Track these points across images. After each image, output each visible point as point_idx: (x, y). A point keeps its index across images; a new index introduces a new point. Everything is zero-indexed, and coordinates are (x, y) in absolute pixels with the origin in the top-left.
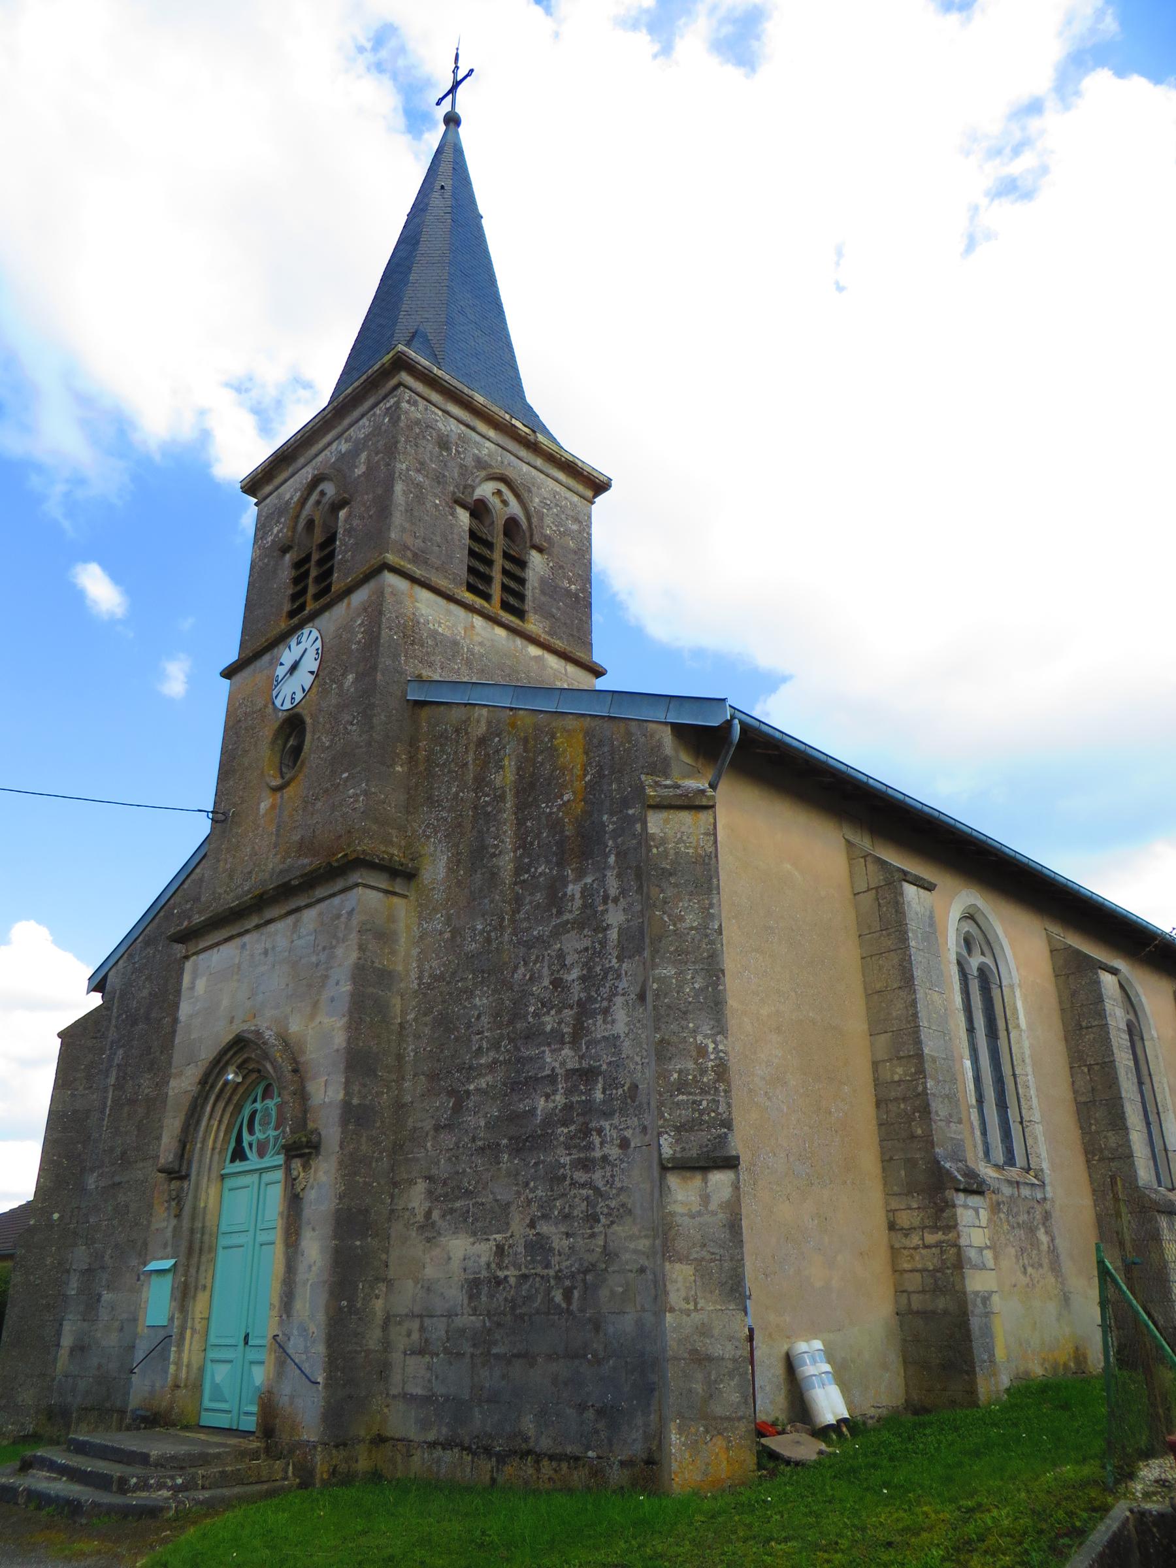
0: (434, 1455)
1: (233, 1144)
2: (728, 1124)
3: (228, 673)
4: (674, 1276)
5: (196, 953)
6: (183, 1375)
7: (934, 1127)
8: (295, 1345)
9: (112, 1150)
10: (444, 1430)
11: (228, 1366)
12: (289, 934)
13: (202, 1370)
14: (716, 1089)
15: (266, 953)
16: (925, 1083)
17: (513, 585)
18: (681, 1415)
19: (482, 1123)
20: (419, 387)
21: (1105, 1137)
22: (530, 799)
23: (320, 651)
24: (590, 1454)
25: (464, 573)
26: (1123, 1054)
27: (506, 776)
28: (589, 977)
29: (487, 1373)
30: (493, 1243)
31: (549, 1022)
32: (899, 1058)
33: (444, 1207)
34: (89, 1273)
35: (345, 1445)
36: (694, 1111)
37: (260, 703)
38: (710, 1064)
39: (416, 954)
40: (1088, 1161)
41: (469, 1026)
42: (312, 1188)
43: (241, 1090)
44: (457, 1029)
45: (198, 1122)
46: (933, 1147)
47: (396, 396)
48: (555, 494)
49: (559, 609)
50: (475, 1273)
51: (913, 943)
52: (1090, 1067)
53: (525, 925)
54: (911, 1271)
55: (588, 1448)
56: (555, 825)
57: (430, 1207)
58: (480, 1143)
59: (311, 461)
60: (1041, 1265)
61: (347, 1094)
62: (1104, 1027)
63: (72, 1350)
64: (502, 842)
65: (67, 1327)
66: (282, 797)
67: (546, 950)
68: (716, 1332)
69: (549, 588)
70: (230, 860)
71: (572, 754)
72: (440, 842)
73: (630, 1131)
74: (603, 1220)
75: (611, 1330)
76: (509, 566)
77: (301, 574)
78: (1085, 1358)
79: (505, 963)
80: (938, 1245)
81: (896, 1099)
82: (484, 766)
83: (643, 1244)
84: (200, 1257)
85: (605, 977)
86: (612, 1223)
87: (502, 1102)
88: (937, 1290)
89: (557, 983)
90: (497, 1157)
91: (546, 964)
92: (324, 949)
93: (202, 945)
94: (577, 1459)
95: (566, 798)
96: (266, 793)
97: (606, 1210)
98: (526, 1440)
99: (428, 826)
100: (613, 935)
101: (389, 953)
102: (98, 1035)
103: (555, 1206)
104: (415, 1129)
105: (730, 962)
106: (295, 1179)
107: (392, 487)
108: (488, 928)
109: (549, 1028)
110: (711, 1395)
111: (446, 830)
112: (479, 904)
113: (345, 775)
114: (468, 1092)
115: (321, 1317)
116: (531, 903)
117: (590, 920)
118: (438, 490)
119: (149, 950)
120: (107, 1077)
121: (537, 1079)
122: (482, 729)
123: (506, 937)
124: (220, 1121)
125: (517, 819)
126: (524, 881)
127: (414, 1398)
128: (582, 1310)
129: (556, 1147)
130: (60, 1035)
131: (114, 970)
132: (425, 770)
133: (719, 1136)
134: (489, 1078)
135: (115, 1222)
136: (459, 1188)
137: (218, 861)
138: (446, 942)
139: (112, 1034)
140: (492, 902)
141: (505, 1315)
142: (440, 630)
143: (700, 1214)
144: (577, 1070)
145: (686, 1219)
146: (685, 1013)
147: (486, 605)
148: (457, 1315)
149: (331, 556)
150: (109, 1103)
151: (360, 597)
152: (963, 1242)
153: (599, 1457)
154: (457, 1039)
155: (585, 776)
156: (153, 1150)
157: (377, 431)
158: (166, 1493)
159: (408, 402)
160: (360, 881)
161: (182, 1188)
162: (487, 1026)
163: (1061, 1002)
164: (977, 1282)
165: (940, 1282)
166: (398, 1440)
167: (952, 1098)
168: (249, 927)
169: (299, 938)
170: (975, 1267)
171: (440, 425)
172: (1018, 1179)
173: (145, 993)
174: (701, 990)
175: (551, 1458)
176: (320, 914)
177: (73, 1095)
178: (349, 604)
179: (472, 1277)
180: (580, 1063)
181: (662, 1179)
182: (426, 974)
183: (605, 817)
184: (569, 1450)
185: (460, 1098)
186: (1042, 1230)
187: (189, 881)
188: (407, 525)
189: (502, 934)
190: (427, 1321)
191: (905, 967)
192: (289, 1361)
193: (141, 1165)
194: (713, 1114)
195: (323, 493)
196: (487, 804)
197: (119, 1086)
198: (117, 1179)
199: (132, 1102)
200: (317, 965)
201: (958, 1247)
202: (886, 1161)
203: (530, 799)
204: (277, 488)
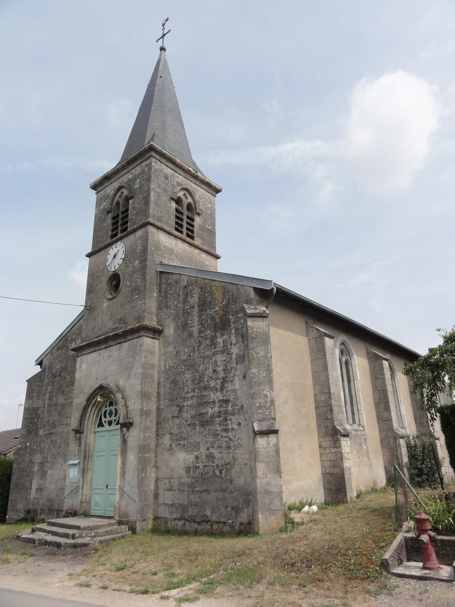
0: (175, 523)
1: (98, 421)
2: (274, 419)
3: (89, 255)
4: (259, 467)
5: (82, 355)
6: (84, 499)
7: (334, 415)
8: (127, 488)
9: (49, 421)
10: (179, 515)
11: (100, 496)
12: (118, 351)
13: (90, 497)
14: (271, 408)
15: (109, 357)
16: (331, 401)
17: (190, 228)
18: (262, 510)
19: (189, 416)
20: (158, 157)
21: (384, 414)
22: (204, 309)
23: (124, 251)
24: (230, 521)
25: (174, 224)
26: (390, 387)
27: (194, 300)
28: (226, 370)
29: (193, 497)
30: (194, 455)
31: (212, 384)
32: (323, 393)
33: (176, 443)
34: (42, 464)
35: (145, 520)
36: (264, 415)
37: (102, 268)
38: (269, 400)
39: (163, 359)
40: (378, 421)
41: (183, 384)
42: (131, 437)
43: (101, 403)
44: (179, 385)
45: (86, 414)
46: (334, 422)
47: (150, 160)
48: (203, 194)
49: (205, 235)
50: (188, 464)
51: (327, 356)
52: (379, 391)
53: (203, 351)
54: (326, 461)
55: (229, 519)
56: (213, 318)
57: (171, 444)
58: (189, 423)
59: (117, 180)
60: (364, 456)
61: (142, 406)
62: (384, 378)
63: (37, 490)
64: (194, 322)
65: (34, 482)
66: (112, 302)
67: (211, 360)
68: (272, 484)
69: (202, 228)
70: (93, 323)
71: (218, 295)
72: (171, 321)
73: (241, 420)
74: (232, 448)
75: (236, 483)
76: (189, 221)
77: (123, 229)
78: (376, 484)
79: (196, 363)
80: (335, 452)
81: (322, 406)
82: (186, 295)
83: (246, 456)
84: (88, 460)
85: (231, 370)
86: (236, 449)
87: (196, 409)
88: (335, 466)
89: (214, 371)
90: (195, 427)
91: (211, 364)
92: (131, 357)
93: (83, 353)
94: (225, 523)
95: (216, 309)
96: (105, 300)
97: (233, 445)
98: (207, 517)
99: (166, 315)
100: (234, 356)
101: (154, 358)
102: (41, 381)
103: (216, 443)
104: (165, 417)
105: (273, 367)
106: (124, 434)
107: (150, 194)
108: (190, 351)
109: (212, 386)
110: (271, 503)
111: (173, 317)
112: (186, 343)
113: (136, 296)
114: (184, 406)
115: (136, 479)
116: (205, 344)
117: (225, 350)
118: (165, 195)
119: (59, 351)
120: (45, 396)
121: (208, 403)
122: (185, 283)
123: (196, 355)
124: (94, 414)
125: (199, 315)
126: (202, 336)
127: (167, 504)
128: (226, 477)
129: (215, 425)
130: (27, 381)
131: (45, 358)
132: (164, 295)
133: (272, 423)
134: (191, 401)
135: (51, 446)
136: (182, 437)
137: (88, 323)
138: (174, 355)
139: (46, 381)
140: (191, 342)
141: (199, 478)
142: (167, 245)
143: (267, 448)
144: (222, 400)
145: (262, 449)
146: (260, 384)
147: (182, 235)
148: (182, 478)
149: (127, 216)
150: (46, 405)
151: (139, 233)
152: (343, 451)
153: (232, 522)
154: (179, 388)
155: (223, 302)
156: (65, 422)
157: (143, 172)
158: (88, 539)
159: (154, 162)
160: (144, 334)
161: (81, 437)
162: (190, 384)
163: (370, 370)
164: (347, 464)
165: (336, 464)
166: (162, 518)
167: (339, 406)
168: (102, 348)
169: (122, 352)
170: (347, 459)
171: (165, 170)
172: (357, 429)
173: (59, 367)
174: (266, 376)
175: (216, 523)
176: (130, 345)
177: (32, 402)
178: (135, 235)
179: (187, 466)
180: (224, 398)
181: (254, 437)
182: (167, 366)
183: (230, 317)
184: (222, 520)
185: (181, 408)
186: (364, 444)
187: (74, 328)
188: (155, 208)
189: (194, 354)
190: (171, 480)
191: (325, 364)
192: (125, 494)
193: (60, 427)
194: (270, 416)
195: (122, 193)
196: (188, 309)
197: (50, 399)
198: (51, 431)
199: (56, 405)
200: (129, 362)
201: (341, 453)
202: (319, 426)
203: (204, 309)
204: (104, 189)
